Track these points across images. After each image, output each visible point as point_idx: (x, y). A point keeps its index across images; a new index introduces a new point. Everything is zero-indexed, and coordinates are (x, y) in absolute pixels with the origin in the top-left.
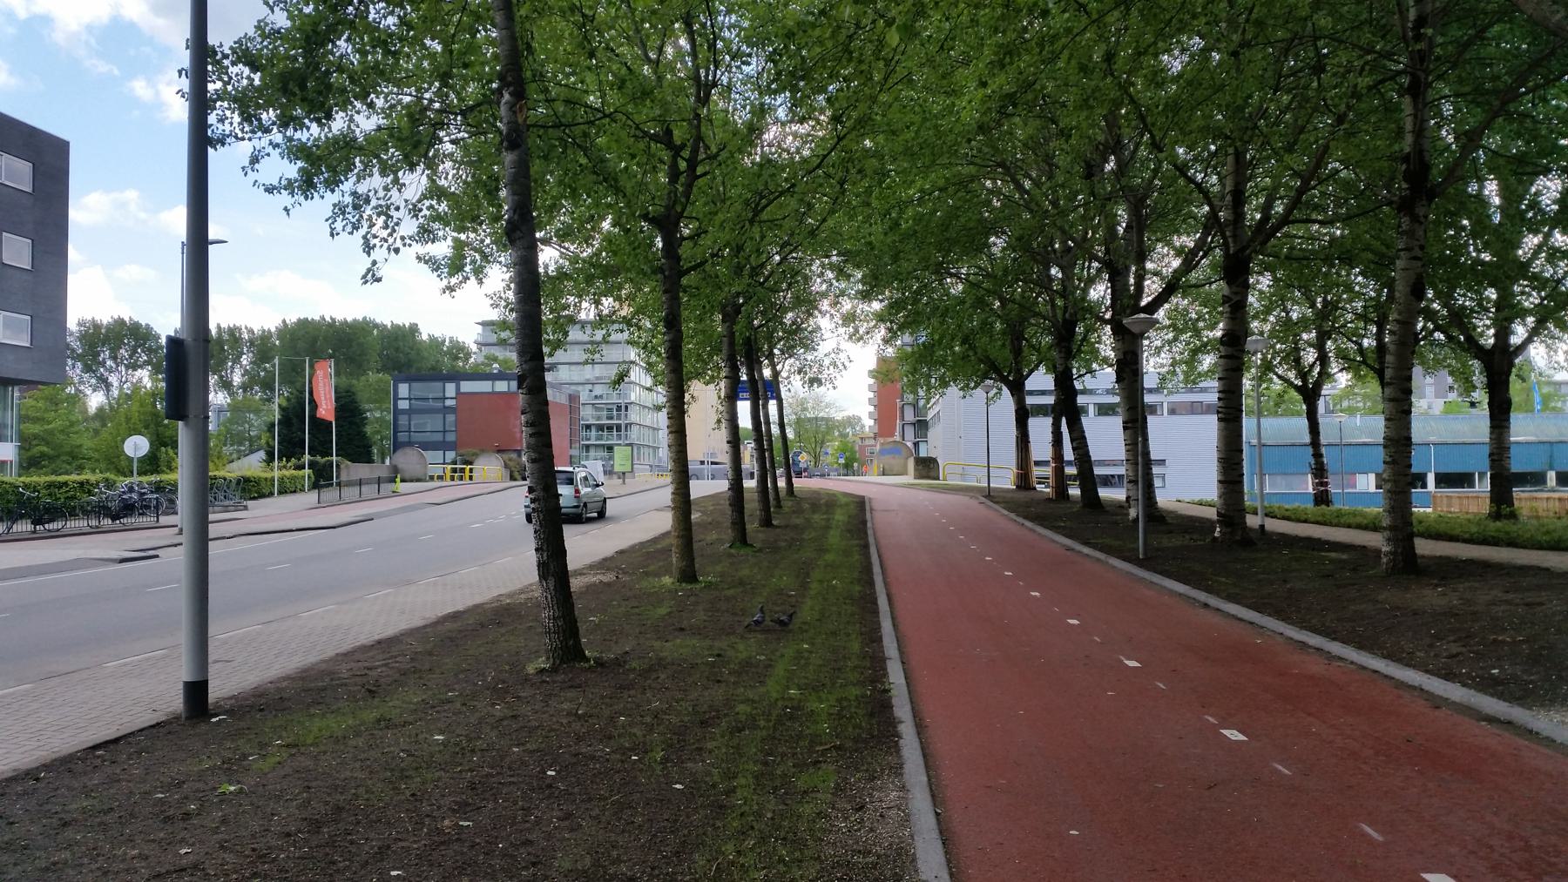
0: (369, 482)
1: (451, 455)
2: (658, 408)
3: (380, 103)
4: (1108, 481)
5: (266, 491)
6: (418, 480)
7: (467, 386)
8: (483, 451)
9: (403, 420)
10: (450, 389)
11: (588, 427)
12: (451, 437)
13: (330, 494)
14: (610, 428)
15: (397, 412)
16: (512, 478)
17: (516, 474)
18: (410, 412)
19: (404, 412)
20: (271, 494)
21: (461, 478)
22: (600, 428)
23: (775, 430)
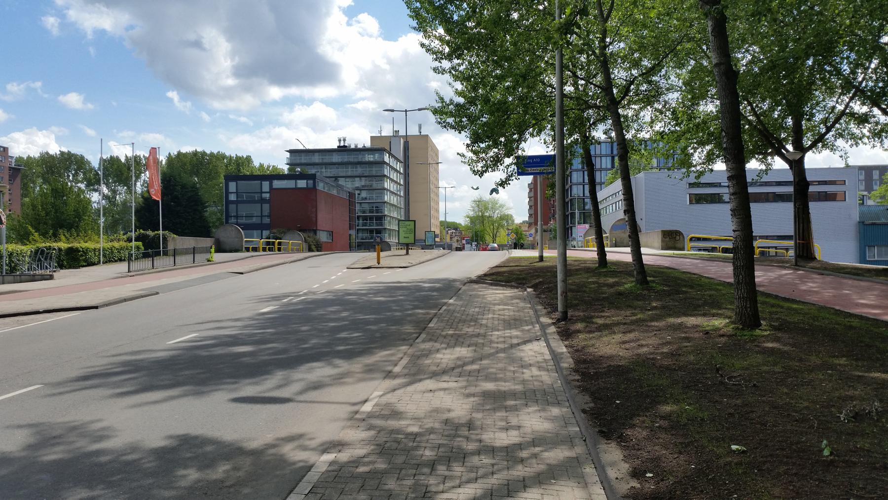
0: (185, 252)
1: (266, 233)
2: (601, 170)
3: (692, 151)
4: (771, 260)
5: (96, 260)
6: (236, 251)
7: (277, 184)
8: (289, 230)
9: (232, 207)
10: (266, 185)
11: (358, 217)
12: (267, 220)
13: (160, 261)
14: (371, 218)
15: (228, 202)
16: (310, 250)
17: (313, 247)
18: (236, 202)
19: (233, 202)
20: (99, 263)
21: (270, 250)
22: (365, 218)
23: (239, 324)
